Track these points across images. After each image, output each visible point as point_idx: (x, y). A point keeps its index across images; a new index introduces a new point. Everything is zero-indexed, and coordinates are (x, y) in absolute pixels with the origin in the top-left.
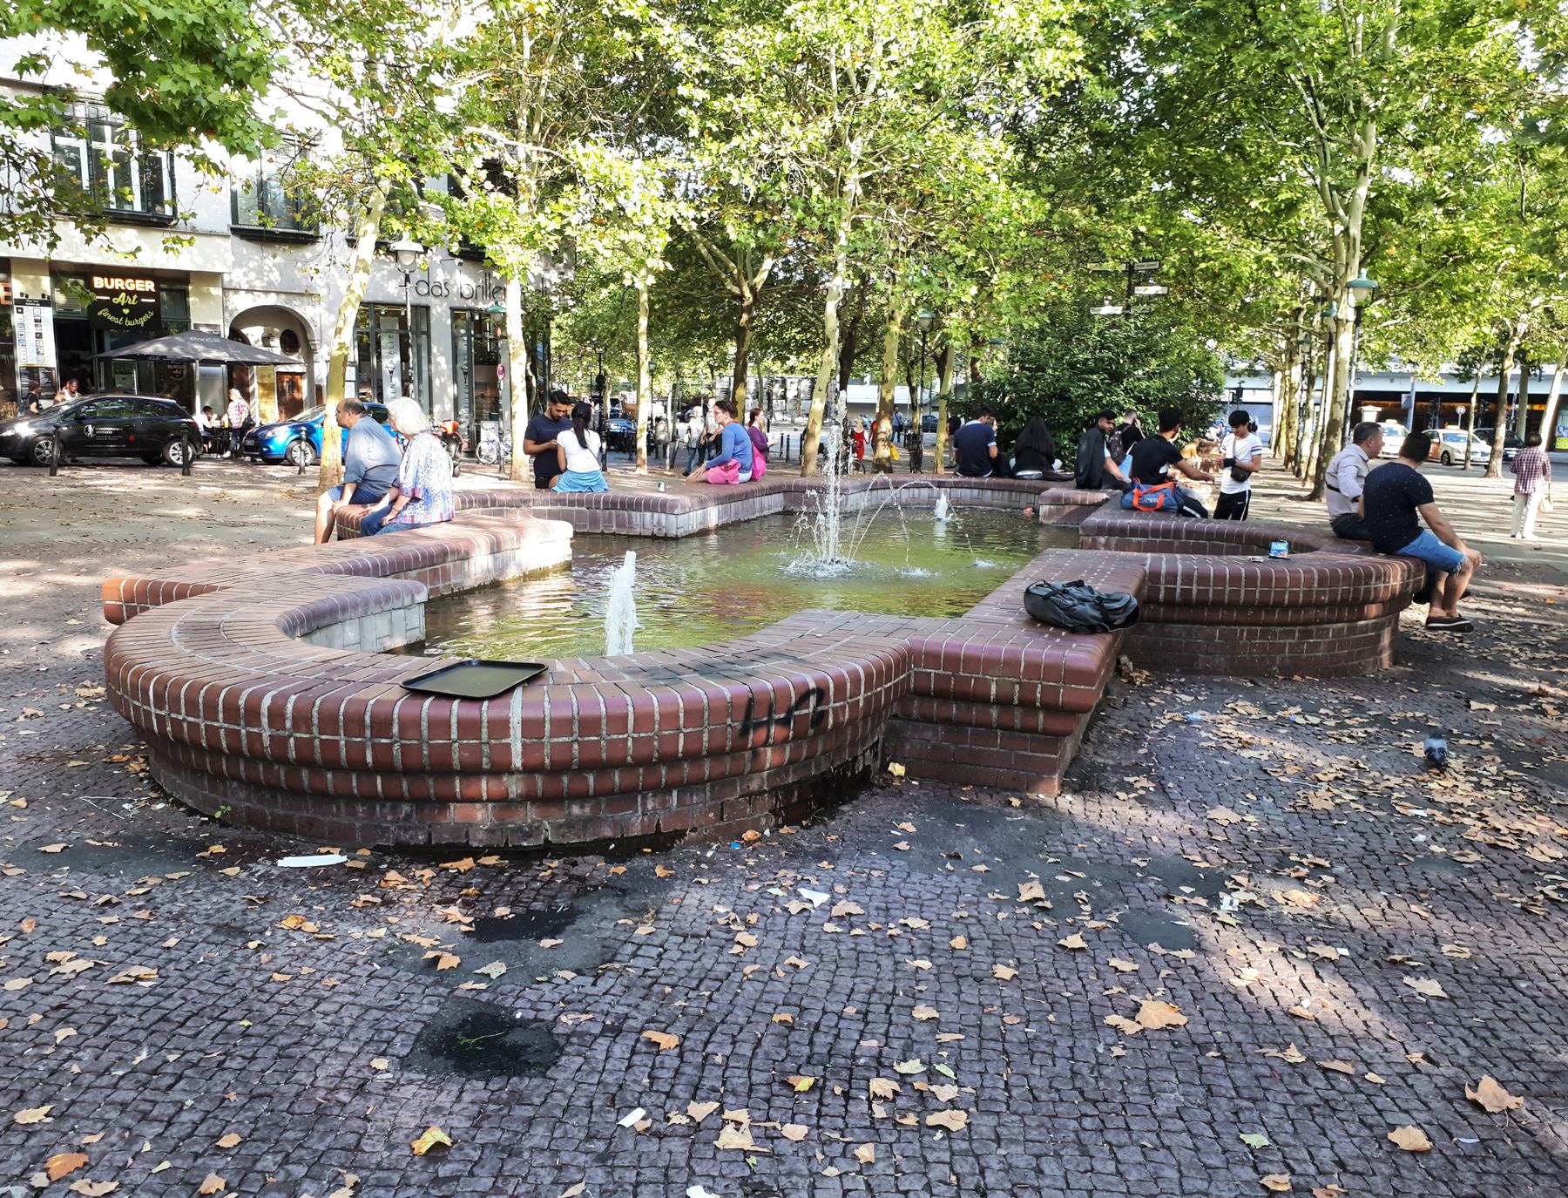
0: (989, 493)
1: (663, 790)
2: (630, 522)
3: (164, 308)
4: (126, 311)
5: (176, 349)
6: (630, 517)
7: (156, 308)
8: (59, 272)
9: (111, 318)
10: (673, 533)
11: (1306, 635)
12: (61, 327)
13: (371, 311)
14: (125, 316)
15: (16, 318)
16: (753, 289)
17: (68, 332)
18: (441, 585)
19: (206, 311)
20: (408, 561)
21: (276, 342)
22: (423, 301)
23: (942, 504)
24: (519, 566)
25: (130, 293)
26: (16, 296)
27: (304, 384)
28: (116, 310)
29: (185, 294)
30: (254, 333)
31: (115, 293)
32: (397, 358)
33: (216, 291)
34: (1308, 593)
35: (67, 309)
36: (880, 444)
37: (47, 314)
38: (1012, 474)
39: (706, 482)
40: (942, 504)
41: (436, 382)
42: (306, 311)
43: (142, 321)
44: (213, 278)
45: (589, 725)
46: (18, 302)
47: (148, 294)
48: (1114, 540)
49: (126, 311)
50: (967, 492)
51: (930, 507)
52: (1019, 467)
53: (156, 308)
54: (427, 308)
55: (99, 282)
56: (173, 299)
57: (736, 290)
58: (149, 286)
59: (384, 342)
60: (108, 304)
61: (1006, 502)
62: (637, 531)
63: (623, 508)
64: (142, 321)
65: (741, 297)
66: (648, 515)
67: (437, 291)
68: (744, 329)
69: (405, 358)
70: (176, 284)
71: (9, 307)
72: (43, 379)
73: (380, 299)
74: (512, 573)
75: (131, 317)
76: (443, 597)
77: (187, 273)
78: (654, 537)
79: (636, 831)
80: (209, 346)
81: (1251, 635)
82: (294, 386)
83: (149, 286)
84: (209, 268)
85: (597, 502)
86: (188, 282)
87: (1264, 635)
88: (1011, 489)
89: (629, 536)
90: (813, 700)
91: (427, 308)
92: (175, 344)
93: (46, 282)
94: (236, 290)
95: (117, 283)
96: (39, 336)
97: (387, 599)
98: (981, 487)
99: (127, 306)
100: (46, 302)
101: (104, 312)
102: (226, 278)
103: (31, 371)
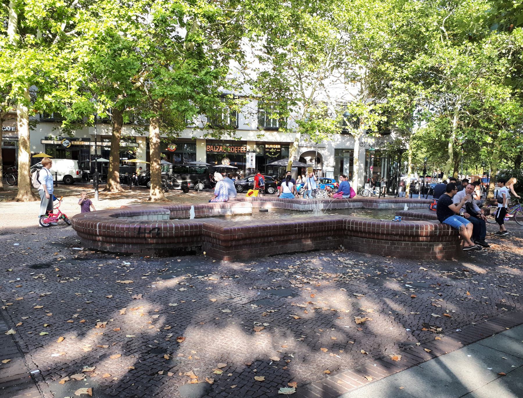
1: (128, 244)
3: (282, 152)
5: (280, 163)
8: (258, 144)
10: (301, 209)
11: (393, 244)
12: (257, 158)
15: (247, 156)
17: (260, 160)
21: (314, 161)
24: (231, 211)
25: (274, 149)
26: (248, 150)
28: (270, 153)
29: (288, 148)
30: (308, 158)
31: (271, 149)
32: (348, 165)
34: (388, 230)
35: (259, 153)
36: (489, 192)
37: (254, 154)
42: (322, 152)
43: (276, 156)
45: (108, 228)
46: (249, 152)
48: (404, 217)
53: (280, 152)
55: (267, 146)
58: (279, 146)
59: (345, 160)
62: (294, 209)
64: (276, 156)
70: (287, 145)
72: (252, 171)
73: (344, 148)
74: (229, 213)
75: (274, 155)
77: (289, 143)
78: (297, 210)
79: (123, 251)
81: (374, 242)
83: (279, 146)
86: (289, 145)
87: (378, 242)
89: (292, 210)
90: (156, 230)
93: (255, 146)
94: (303, 147)
95: (271, 146)
96: (252, 160)
97: (157, 212)
100: (254, 152)
101: (267, 154)
103: (249, 169)
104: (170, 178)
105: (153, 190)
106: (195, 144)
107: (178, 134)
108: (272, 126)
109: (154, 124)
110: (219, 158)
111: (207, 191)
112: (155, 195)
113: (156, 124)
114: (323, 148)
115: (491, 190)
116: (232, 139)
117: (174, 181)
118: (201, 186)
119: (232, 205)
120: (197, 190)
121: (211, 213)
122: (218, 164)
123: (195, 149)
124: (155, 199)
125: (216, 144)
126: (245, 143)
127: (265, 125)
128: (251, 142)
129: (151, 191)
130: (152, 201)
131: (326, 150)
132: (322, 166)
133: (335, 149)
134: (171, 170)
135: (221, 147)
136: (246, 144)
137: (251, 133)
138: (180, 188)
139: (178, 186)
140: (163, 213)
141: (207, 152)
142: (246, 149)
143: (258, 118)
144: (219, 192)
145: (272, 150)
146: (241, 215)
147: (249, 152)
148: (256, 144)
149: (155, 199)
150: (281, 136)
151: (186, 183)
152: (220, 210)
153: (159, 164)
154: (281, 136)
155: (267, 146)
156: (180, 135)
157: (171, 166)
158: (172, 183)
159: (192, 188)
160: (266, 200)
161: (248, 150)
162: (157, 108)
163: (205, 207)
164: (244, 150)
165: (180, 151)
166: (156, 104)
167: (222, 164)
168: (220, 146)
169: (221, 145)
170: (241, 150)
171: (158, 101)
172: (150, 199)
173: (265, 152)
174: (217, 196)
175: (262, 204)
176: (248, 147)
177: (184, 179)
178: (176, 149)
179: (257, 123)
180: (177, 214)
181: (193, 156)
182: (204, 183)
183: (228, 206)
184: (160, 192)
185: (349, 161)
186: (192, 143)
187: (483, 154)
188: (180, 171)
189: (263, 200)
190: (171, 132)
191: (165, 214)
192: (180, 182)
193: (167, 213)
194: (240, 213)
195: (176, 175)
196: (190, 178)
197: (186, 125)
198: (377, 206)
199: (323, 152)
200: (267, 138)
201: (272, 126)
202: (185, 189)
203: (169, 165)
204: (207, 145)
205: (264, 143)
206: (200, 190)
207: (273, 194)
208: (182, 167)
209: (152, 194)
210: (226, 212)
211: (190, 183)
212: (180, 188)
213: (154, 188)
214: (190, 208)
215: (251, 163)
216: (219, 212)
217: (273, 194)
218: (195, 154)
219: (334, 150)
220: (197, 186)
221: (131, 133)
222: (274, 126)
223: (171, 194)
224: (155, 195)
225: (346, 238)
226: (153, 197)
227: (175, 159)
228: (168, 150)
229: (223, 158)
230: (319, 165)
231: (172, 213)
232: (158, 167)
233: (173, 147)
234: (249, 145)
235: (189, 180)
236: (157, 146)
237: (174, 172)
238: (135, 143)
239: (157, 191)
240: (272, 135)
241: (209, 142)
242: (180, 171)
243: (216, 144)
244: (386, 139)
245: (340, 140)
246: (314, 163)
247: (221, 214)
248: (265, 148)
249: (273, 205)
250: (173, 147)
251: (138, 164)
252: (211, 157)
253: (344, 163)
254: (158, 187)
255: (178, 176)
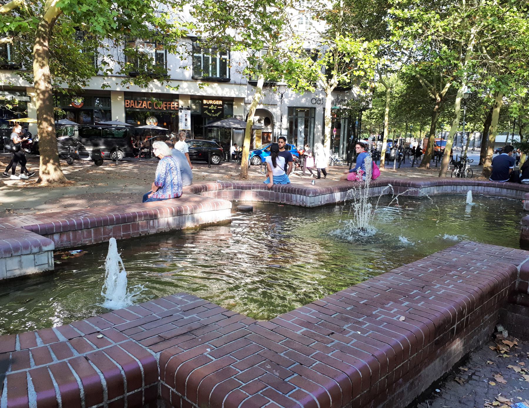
0: (505, 190)
2: (291, 199)
3: (225, 110)
4: (213, 111)
5: (224, 124)
6: (291, 196)
7: (222, 110)
8: (193, 98)
9: (208, 114)
12: (192, 116)
13: (292, 110)
14: (212, 113)
15: (180, 114)
16: (440, 96)
17: (196, 119)
18: (131, 232)
19: (238, 111)
20: (52, 228)
21: (263, 122)
22: (313, 106)
23: (469, 194)
24: (193, 219)
25: (214, 105)
26: (180, 107)
27: (271, 135)
29: (232, 105)
32: (303, 127)
33: (242, 104)
35: (195, 111)
36: (487, 160)
37: (189, 112)
38: (519, 181)
39: (346, 180)
40: (469, 194)
41: (316, 135)
43: (217, 115)
44: (242, 99)
46: (182, 109)
47: (220, 105)
49: (213, 111)
50: (494, 189)
51: (463, 197)
52: (523, 178)
53: (222, 110)
54: (315, 108)
55: (205, 102)
56: (228, 107)
57: (433, 97)
58: (221, 102)
59: (299, 120)
60: (207, 109)
61: (514, 196)
62: (294, 203)
63: (289, 192)
64: (217, 115)
65: (435, 99)
66: (299, 196)
67: (319, 102)
68: (435, 112)
69: (306, 127)
70: (229, 101)
71: (178, 111)
73: (299, 106)
75: (214, 113)
76: (133, 239)
77: (233, 98)
78: (300, 207)
80: (235, 123)
82: (268, 136)
83: (221, 102)
84: (240, 96)
85: (279, 189)
86: (233, 101)
88: (517, 189)
91: (290, 108)
92: (224, 122)
93: (190, 101)
95: (211, 102)
96: (186, 120)
98: (501, 187)
99: (213, 109)
100: (188, 109)
101: (206, 112)
102: (246, 99)
104: (74, 145)
105: (44, 167)
106: (110, 98)
107: (84, 82)
108: (210, 76)
109: (40, 59)
110: (143, 117)
111: (129, 162)
112: (49, 173)
113: (43, 59)
114: (274, 105)
115: (488, 157)
116: (160, 91)
117: (81, 148)
118: (120, 155)
119: (195, 208)
120: (114, 160)
121: (153, 227)
122: (140, 125)
123: (110, 104)
124: (48, 181)
125: (138, 99)
126: (176, 97)
127: (203, 73)
128: (184, 97)
129: (42, 168)
130: (44, 183)
131: (278, 108)
132: (273, 128)
133: (290, 108)
134: (77, 133)
135: (145, 102)
136: (178, 99)
137: (185, 85)
138: (89, 158)
139: (87, 155)
140: (35, 250)
141: (126, 108)
142: (178, 105)
143: (193, 65)
144: (165, 179)
145: (212, 107)
146: (212, 225)
147: (182, 109)
148: (191, 99)
149: (48, 181)
150: (223, 89)
151: (99, 151)
152: (171, 220)
153: (51, 125)
154: (223, 89)
155: (205, 102)
156: (87, 83)
157: (76, 128)
158: (77, 152)
159: (108, 158)
160: (243, 188)
161: (180, 107)
162: (45, 33)
163: (140, 216)
164: (176, 106)
165: (89, 108)
166: (43, 26)
167: (146, 124)
168: (143, 100)
169: (144, 100)
170: (172, 106)
171: (46, 22)
172: (40, 181)
173: (203, 110)
174: (160, 188)
175: (237, 195)
176: (181, 103)
177: (96, 145)
178: (84, 102)
179: (192, 71)
180: (75, 237)
181: (107, 114)
182: (125, 150)
183: (186, 210)
184: (55, 170)
185: (304, 122)
186: (106, 96)
187: (514, 111)
188: (89, 134)
189: (239, 188)
190: (75, 80)
191: (41, 251)
192: (89, 149)
193: (45, 248)
194: (210, 221)
195: (84, 140)
196: (105, 144)
197: (95, 72)
198: (416, 192)
199: (275, 111)
200: (206, 91)
201: (210, 76)
202: (98, 160)
203: (73, 126)
204: (125, 99)
205: (202, 98)
206: (119, 160)
207: (218, 164)
208: (93, 128)
209: (43, 173)
210: (184, 223)
211: (104, 150)
212: (89, 158)
213: (45, 163)
214: (104, 247)
215: (185, 122)
216: (168, 224)
217: (218, 164)
218: (110, 111)
219: (287, 108)
220: (114, 155)
221: (18, 81)
222: (214, 76)
223: (77, 168)
224: (49, 173)
225: (515, 311)
226: (44, 178)
227: (84, 118)
228: (73, 106)
229: (146, 118)
230: (269, 127)
231: (65, 238)
232: (50, 129)
233: (79, 102)
234: (182, 100)
235: (103, 147)
236: (47, 95)
237: (81, 135)
238: (25, 95)
239: (51, 167)
240: (212, 88)
241: (128, 95)
242: (89, 134)
243: (138, 99)
244: (347, 96)
245: (294, 96)
246: (263, 125)
247: (173, 226)
248: (202, 104)
249: (257, 195)
250: (79, 102)
251: (30, 125)
252: (130, 115)
253: (299, 124)
254: (51, 161)
255: (87, 140)
